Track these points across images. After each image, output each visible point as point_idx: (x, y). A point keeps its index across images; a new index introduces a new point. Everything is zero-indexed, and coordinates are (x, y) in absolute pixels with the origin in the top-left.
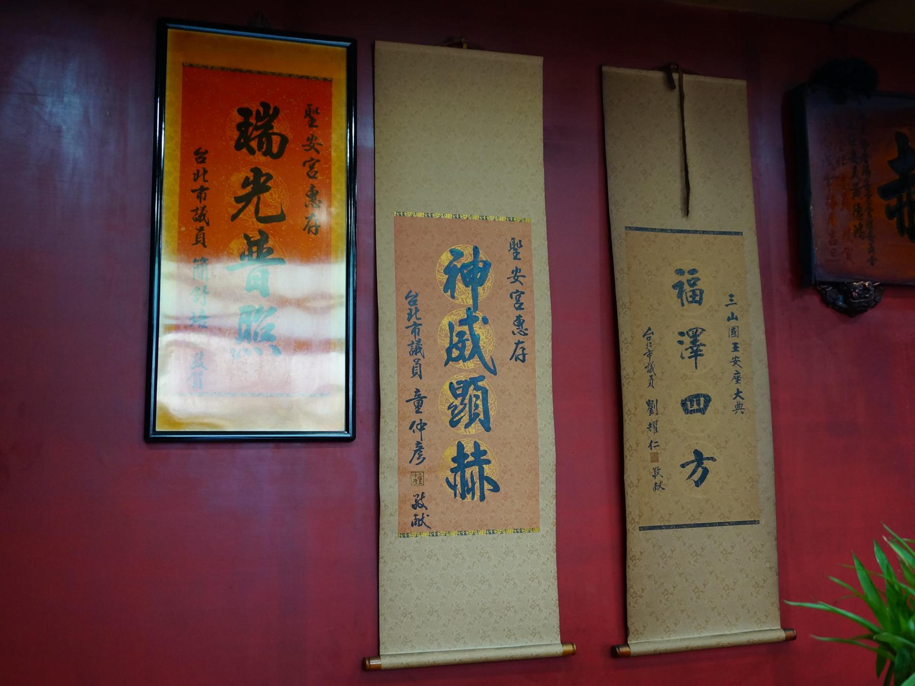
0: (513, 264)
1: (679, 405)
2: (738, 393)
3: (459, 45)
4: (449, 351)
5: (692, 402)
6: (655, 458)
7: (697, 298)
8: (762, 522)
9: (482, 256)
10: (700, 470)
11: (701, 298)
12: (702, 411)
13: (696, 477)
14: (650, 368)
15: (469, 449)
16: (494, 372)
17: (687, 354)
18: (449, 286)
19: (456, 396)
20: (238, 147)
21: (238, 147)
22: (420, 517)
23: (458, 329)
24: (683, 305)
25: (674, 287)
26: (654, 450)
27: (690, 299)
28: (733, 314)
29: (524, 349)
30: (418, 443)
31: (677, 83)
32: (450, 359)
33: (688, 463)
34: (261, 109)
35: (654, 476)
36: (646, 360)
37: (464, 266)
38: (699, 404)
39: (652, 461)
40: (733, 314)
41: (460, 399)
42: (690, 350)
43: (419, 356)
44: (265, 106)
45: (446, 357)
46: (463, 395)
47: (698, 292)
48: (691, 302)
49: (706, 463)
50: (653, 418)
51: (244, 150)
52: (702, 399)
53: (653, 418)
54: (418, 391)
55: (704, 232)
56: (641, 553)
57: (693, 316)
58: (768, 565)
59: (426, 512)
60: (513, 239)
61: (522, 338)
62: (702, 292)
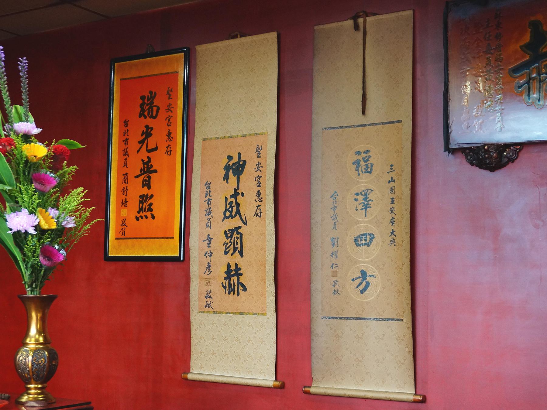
0: (257, 160)
1: (353, 240)
2: (393, 232)
3: (235, 37)
4: (225, 213)
5: (361, 238)
6: (335, 274)
7: (369, 170)
8: (405, 320)
9: (242, 159)
10: (364, 283)
11: (371, 169)
12: (368, 245)
13: (361, 288)
14: (335, 217)
15: (233, 267)
16: (246, 224)
17: (360, 207)
18: (226, 177)
19: (227, 238)
20: (140, 116)
21: (140, 116)
22: (209, 303)
23: (229, 200)
24: (359, 175)
25: (353, 164)
26: (334, 269)
27: (364, 171)
28: (392, 178)
29: (260, 209)
30: (209, 263)
31: (362, 28)
32: (225, 217)
33: (356, 279)
34: (149, 95)
35: (334, 286)
36: (332, 212)
37: (234, 164)
38: (366, 240)
39: (333, 276)
40: (392, 178)
41: (230, 239)
42: (362, 204)
43: (210, 216)
44: (151, 92)
45: (223, 216)
46: (231, 237)
47: (370, 166)
48: (365, 172)
49: (369, 279)
50: (335, 249)
51: (143, 117)
52: (368, 237)
53: (335, 249)
54: (209, 235)
55: (376, 124)
56: (322, 332)
57: (364, 182)
58: (407, 349)
59: (212, 301)
60: (258, 146)
61: (259, 203)
62: (372, 165)
